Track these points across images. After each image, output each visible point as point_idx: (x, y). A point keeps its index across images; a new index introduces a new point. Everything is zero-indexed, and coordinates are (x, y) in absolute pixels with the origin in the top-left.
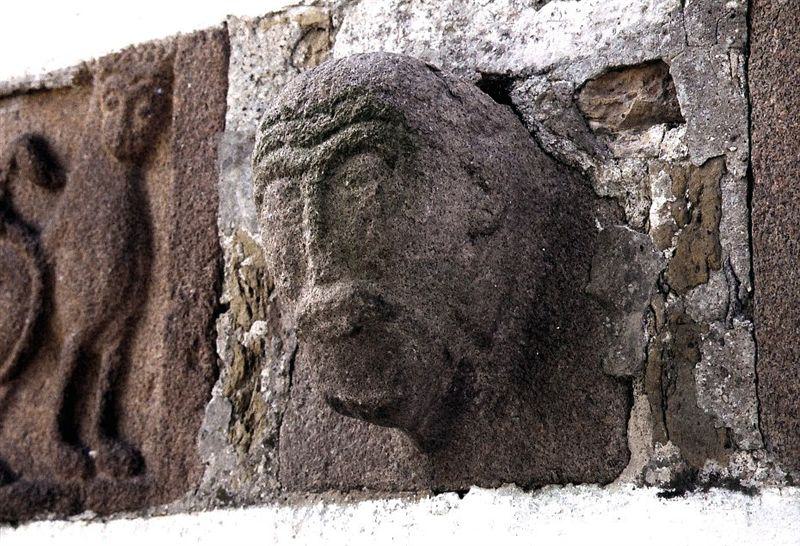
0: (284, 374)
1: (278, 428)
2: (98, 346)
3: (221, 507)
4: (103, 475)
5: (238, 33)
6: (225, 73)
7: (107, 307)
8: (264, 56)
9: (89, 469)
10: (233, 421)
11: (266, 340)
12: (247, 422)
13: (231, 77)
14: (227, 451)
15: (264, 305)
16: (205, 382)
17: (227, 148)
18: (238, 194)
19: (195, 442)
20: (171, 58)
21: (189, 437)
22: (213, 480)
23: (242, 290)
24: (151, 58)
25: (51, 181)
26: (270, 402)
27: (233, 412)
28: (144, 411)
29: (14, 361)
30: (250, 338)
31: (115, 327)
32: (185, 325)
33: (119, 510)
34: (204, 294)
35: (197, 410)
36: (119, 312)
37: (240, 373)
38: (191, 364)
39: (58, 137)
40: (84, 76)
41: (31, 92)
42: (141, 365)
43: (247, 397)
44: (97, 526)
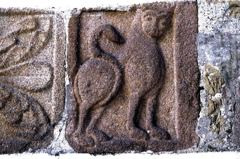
0: (231, 110)
1: (231, 127)
2: (147, 96)
3: (211, 151)
4: (153, 139)
5: (202, 3)
6: (197, 15)
7: (152, 84)
8: (214, 11)
9: (148, 137)
10: (211, 124)
11: (222, 99)
12: (217, 124)
13: (200, 16)
14: (211, 133)
15: (219, 88)
16: (196, 111)
17: (200, 39)
18: (206, 53)
19: (195, 130)
20: (174, 7)
21: (193, 128)
22: (205, 143)
23: (210, 83)
24: (165, 7)
25: (120, 41)
26: (226, 119)
27: (211, 122)
28: (168, 119)
29: (109, 99)
30: (215, 98)
31: (154, 91)
32: (187, 92)
33: (163, 150)
34: (194, 83)
35: (194, 120)
36: (156, 86)
37: (212, 109)
38: (190, 105)
39: (119, 26)
40: (133, 9)
41: (110, 11)
42: (164, 104)
43: (216, 117)
44: (155, 156)
